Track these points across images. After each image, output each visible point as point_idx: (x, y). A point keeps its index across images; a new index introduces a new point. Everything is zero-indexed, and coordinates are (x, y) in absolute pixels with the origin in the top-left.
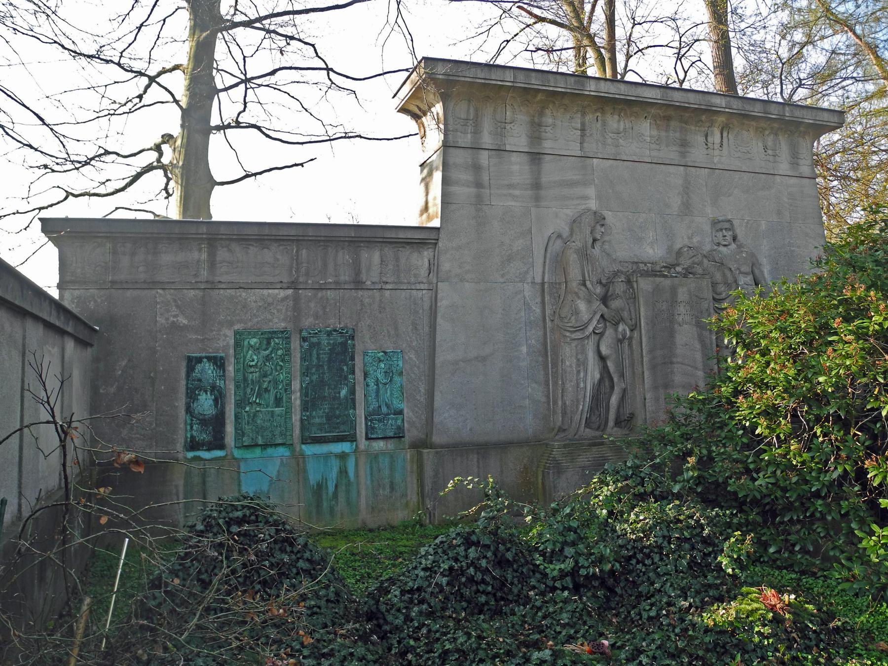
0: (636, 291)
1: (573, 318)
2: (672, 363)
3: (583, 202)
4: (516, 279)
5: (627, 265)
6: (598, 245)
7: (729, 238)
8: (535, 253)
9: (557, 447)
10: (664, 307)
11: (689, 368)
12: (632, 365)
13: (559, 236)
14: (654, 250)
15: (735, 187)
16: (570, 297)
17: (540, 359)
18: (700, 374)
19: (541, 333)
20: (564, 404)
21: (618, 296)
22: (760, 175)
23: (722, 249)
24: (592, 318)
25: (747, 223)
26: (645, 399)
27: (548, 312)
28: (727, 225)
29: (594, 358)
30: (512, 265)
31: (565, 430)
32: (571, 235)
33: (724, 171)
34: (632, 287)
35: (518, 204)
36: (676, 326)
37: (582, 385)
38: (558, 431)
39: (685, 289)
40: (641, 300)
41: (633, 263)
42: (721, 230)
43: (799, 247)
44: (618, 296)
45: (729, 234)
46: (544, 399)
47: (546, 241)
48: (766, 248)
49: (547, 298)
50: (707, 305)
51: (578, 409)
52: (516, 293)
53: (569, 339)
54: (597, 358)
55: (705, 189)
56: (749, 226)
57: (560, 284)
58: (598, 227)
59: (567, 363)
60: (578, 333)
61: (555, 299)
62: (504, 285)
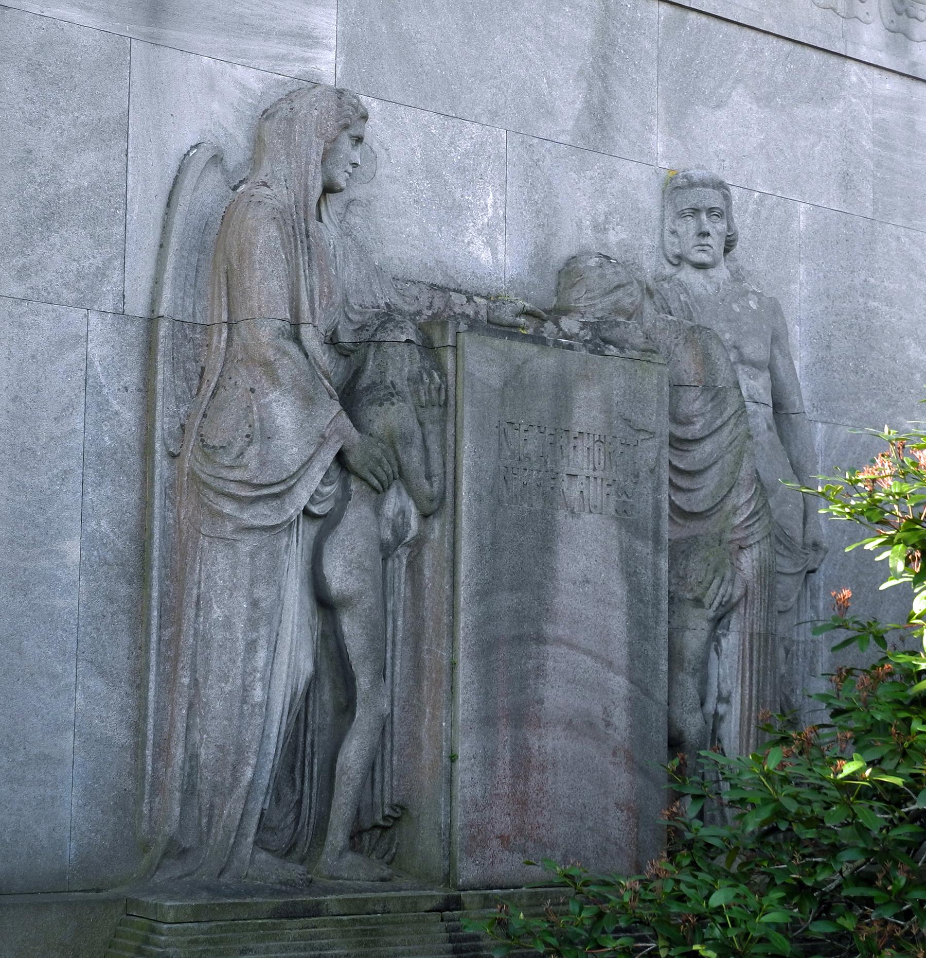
0: (451, 379)
1: (253, 450)
2: (540, 639)
3: (298, 51)
4: (65, 293)
5: (415, 291)
6: (335, 203)
7: (716, 242)
8: (135, 208)
9: (170, 916)
10: (531, 447)
11: (589, 661)
12: (416, 637)
13: (217, 159)
14: (494, 253)
15: (738, 81)
16: (242, 378)
17: (123, 590)
18: (619, 683)
19: (130, 498)
20: (192, 757)
21: (392, 393)
22: (808, 51)
23: (688, 275)
24: (311, 459)
25: (760, 202)
26: (453, 759)
27: (163, 424)
28: (713, 199)
29: (301, 601)
30: (55, 239)
31: (184, 852)
32: (254, 162)
33: (713, 23)
34: (440, 368)
35: (90, 20)
36: (561, 515)
37: (258, 694)
38: (165, 854)
39: (595, 392)
40: (467, 413)
41: (433, 287)
42: (696, 211)
43: (889, 302)
44: (392, 393)
45: (717, 228)
46: (122, 736)
47: (171, 172)
48: (805, 292)
49: (163, 372)
50: (652, 455)
51: (236, 780)
52: (61, 343)
53: (229, 527)
54: (308, 603)
55: (653, 74)
56: (764, 214)
57: (206, 328)
58: (346, 143)
59: (217, 613)
60: (262, 508)
61: (187, 380)
62: (24, 308)
